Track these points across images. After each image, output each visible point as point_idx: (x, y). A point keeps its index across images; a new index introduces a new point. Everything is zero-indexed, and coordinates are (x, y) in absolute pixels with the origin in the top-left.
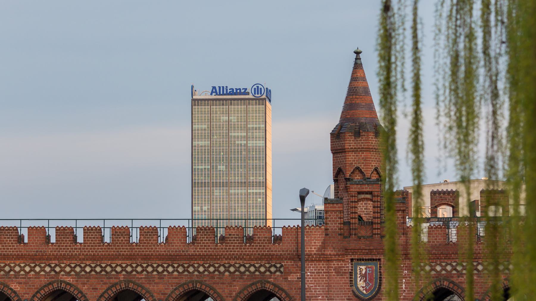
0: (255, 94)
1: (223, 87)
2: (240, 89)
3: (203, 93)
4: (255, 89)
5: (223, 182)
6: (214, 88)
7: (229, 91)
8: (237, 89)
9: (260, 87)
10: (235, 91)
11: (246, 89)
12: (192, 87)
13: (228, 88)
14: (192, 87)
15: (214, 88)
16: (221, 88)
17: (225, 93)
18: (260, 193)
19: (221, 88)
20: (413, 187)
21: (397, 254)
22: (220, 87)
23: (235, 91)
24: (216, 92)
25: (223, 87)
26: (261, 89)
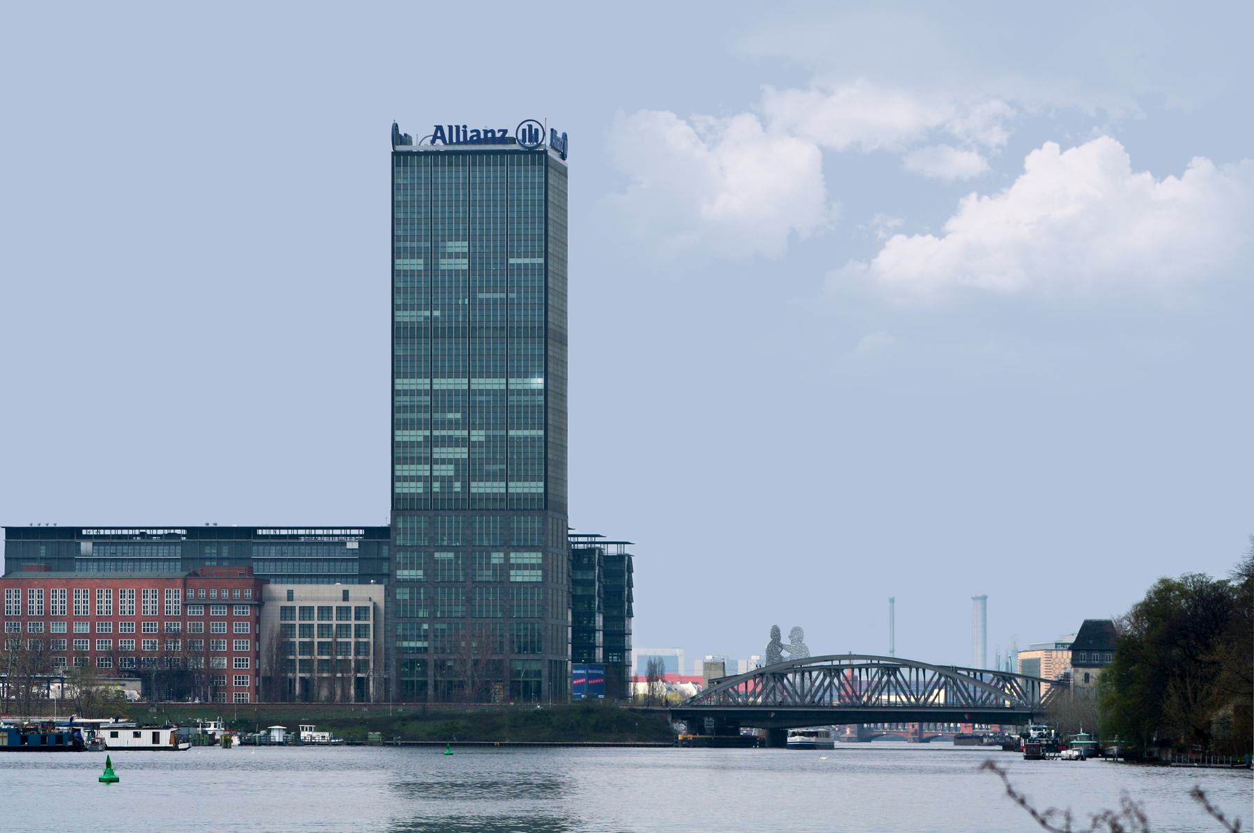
1: (458, 127)
2: (492, 131)
3: (421, 139)
4: (524, 131)
6: (439, 128)
7: (469, 135)
8: (486, 132)
9: (535, 126)
11: (505, 131)
13: (468, 130)
15: (439, 128)
22: (450, 127)
24: (443, 138)
26: (537, 130)
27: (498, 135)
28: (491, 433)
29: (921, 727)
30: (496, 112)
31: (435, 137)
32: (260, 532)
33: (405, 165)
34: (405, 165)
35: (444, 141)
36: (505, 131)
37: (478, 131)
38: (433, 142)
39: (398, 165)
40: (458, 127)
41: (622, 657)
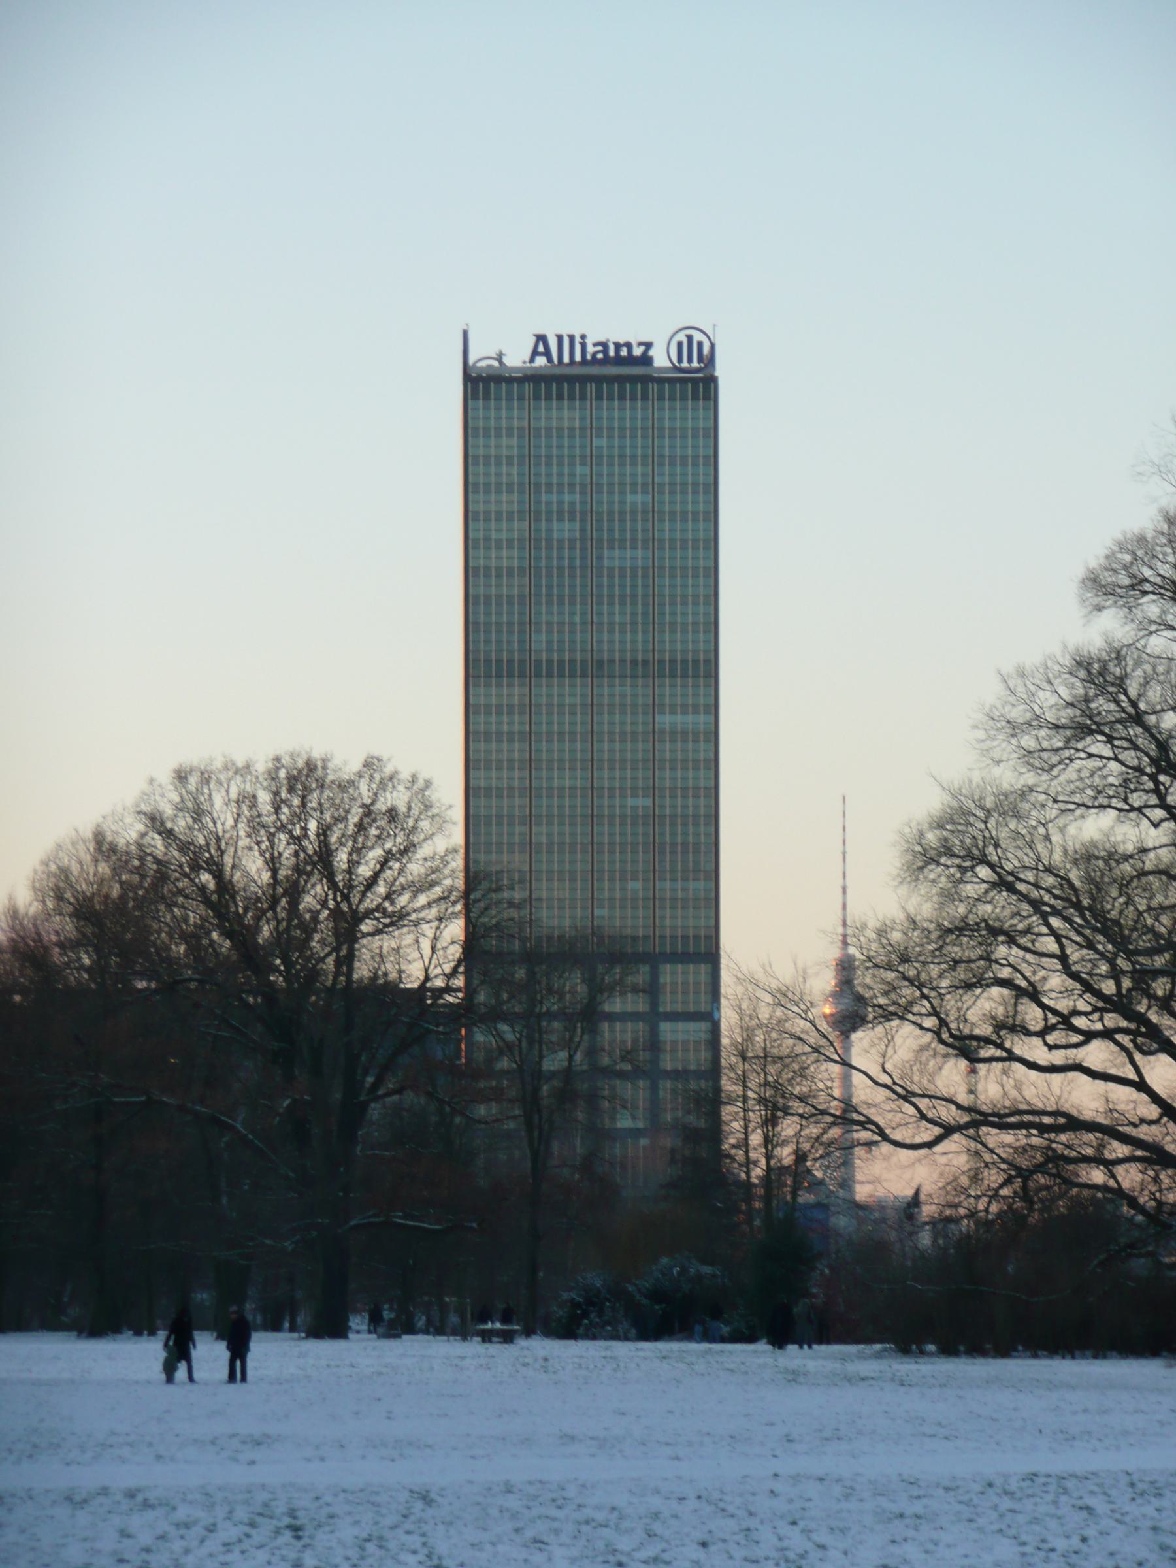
0: (680, 360)
1: (572, 338)
2: (629, 345)
4: (680, 344)
5: (572, 661)
7: (591, 349)
8: (618, 346)
9: (698, 337)
10: (612, 353)
11: (648, 345)
12: (465, 334)
13: (589, 342)
14: (465, 334)
15: (541, 338)
16: (239, 1375)
17: (578, 358)
18: (673, 712)
19: (239, 1375)
20: (1157, 727)
21: (576, 928)
22: (560, 338)
23: (612, 353)
26: (700, 344)
27: (638, 351)
28: (567, 902)
29: (972, 1030)
30: (646, 323)
31: (535, 353)
32: (238, 1363)
33: (486, 397)
34: (486, 397)
35: (550, 359)
36: (648, 345)
38: (532, 360)
39: (707, 662)
40: (572, 338)
41: (454, 1333)
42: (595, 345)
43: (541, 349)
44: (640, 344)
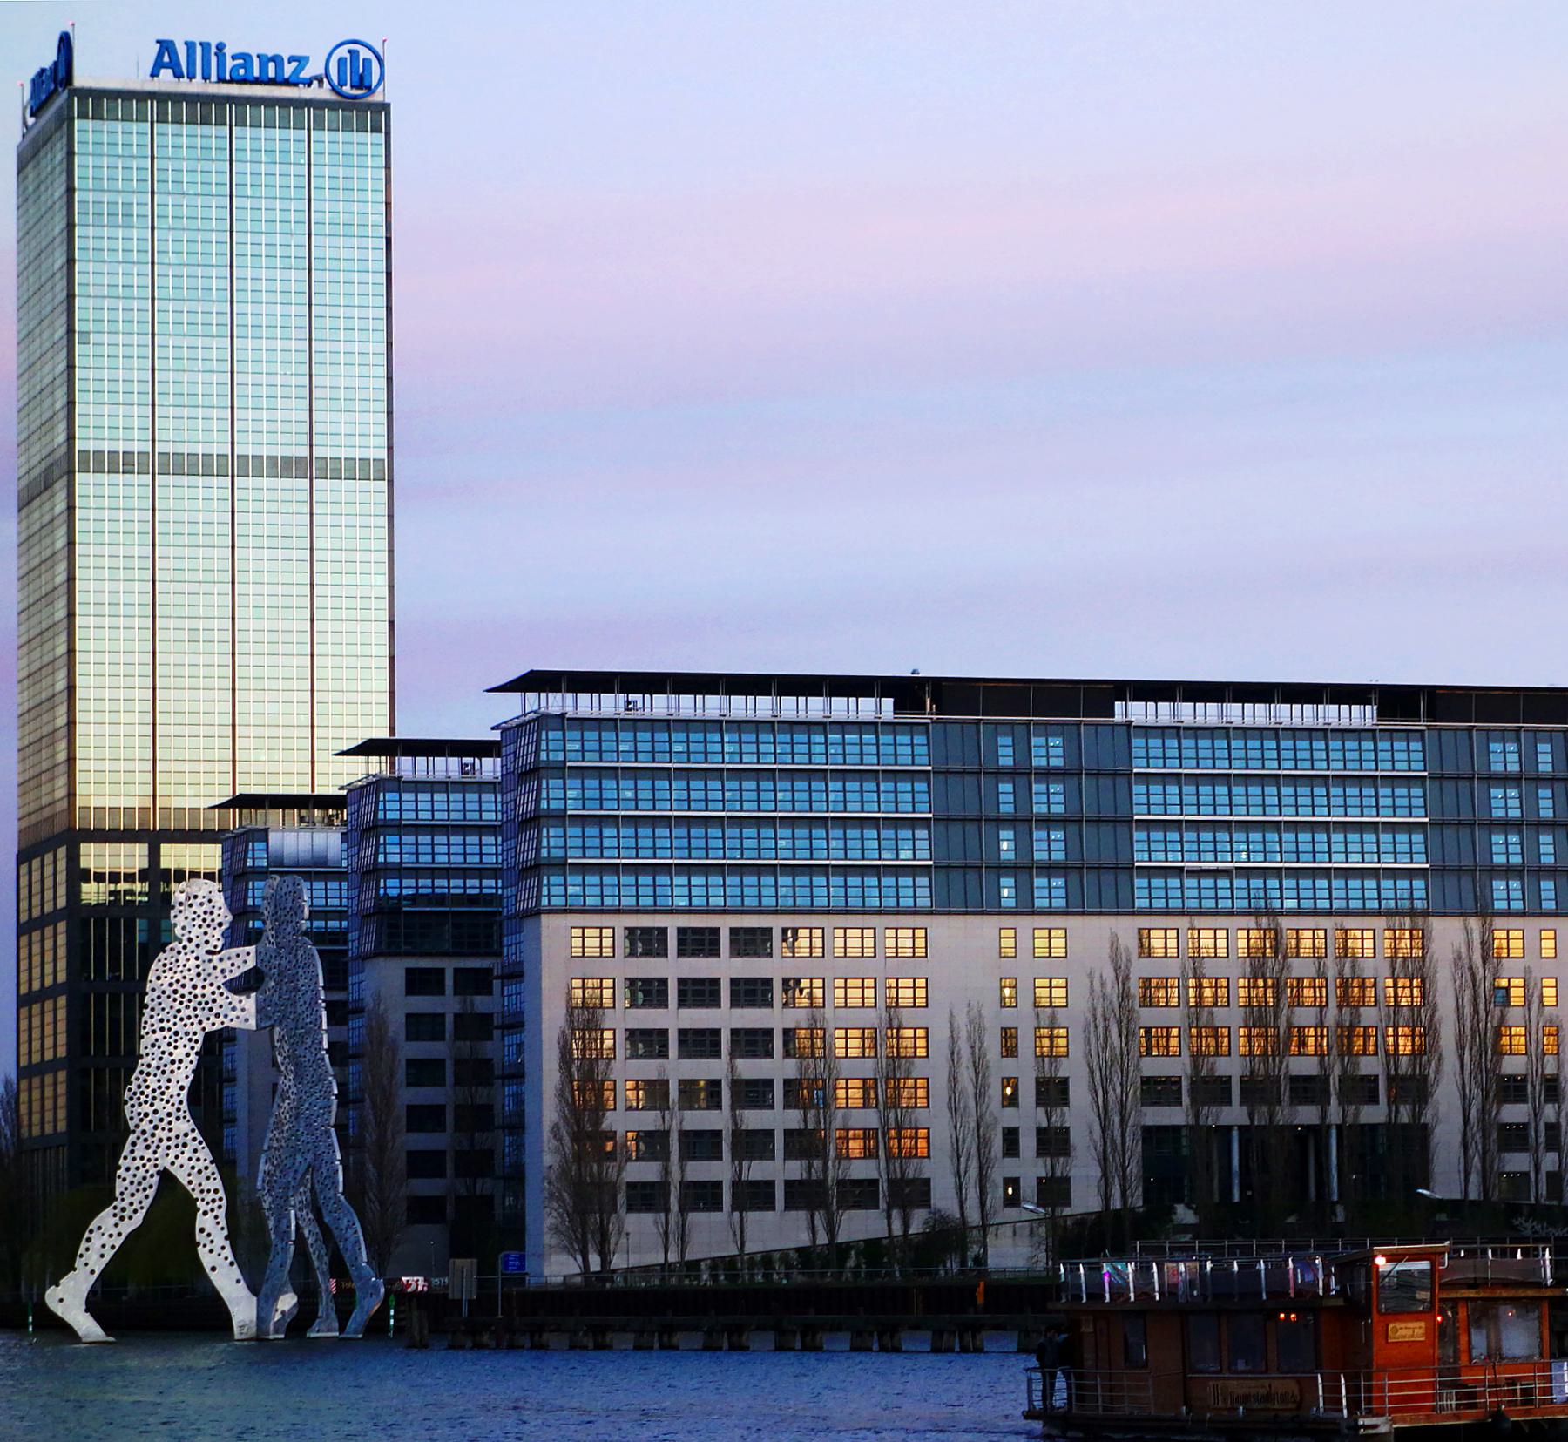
4: (341, 61)
6: (166, 46)
7: (230, 64)
9: (364, 53)
13: (229, 51)
15: (166, 46)
22: (190, 46)
25: (205, 46)
35: (178, 75)
37: (246, 57)
38: (154, 74)
42: (233, 58)
43: (166, 59)
44: (291, 60)
